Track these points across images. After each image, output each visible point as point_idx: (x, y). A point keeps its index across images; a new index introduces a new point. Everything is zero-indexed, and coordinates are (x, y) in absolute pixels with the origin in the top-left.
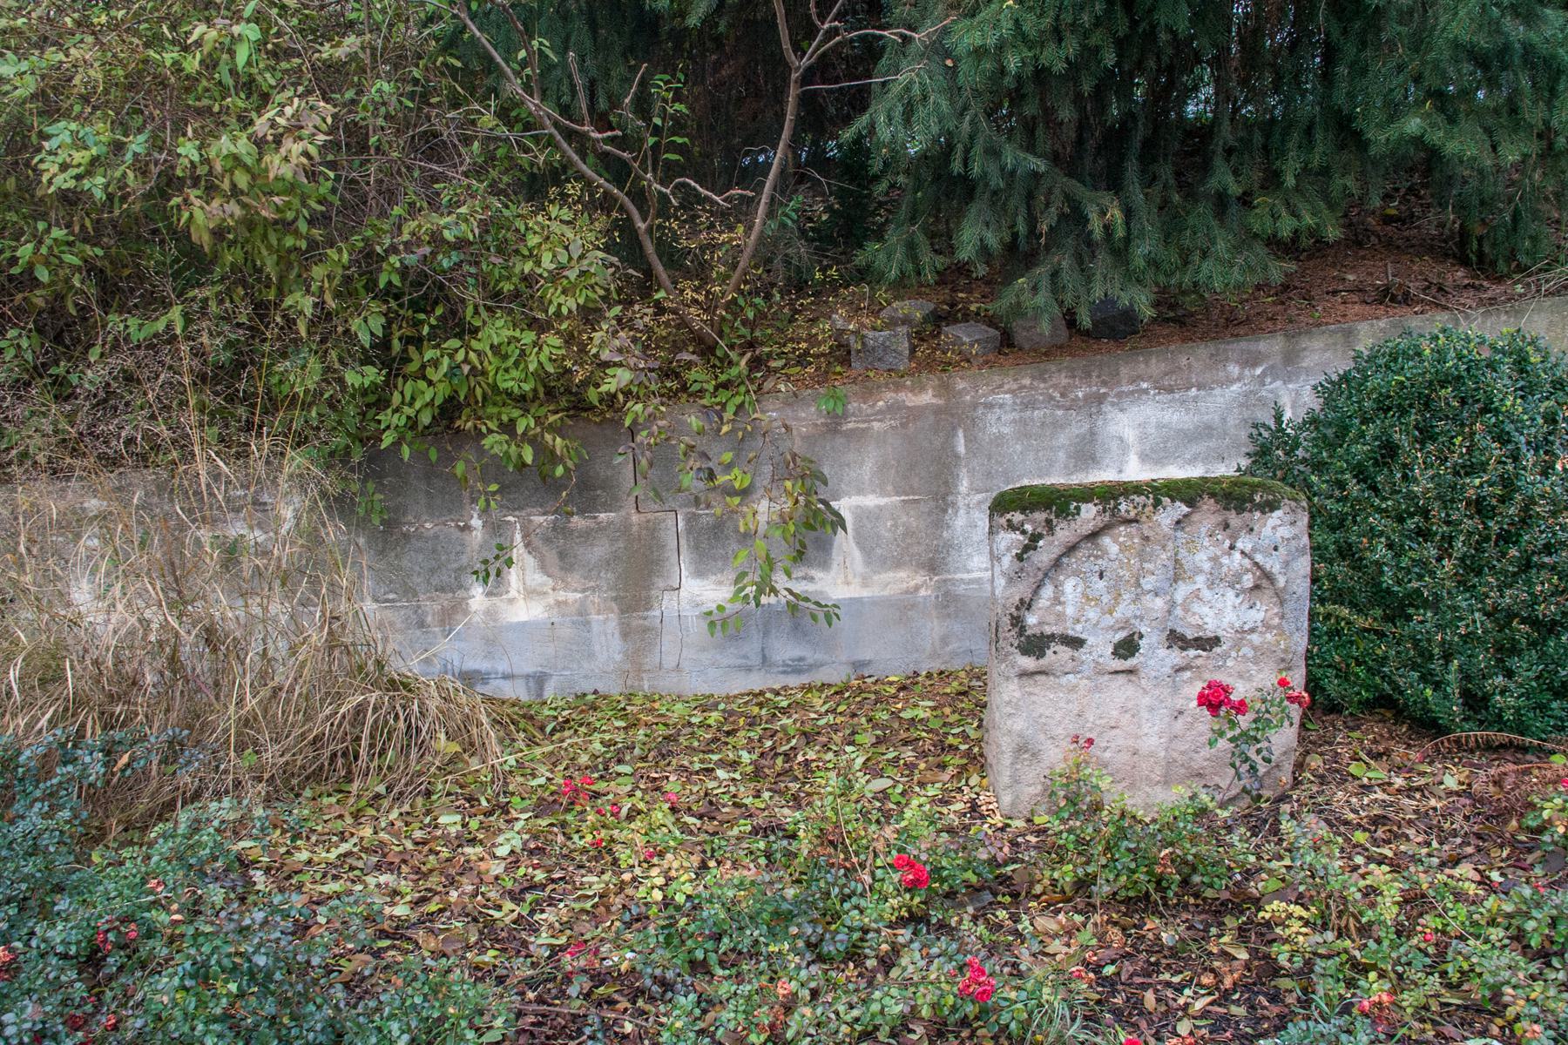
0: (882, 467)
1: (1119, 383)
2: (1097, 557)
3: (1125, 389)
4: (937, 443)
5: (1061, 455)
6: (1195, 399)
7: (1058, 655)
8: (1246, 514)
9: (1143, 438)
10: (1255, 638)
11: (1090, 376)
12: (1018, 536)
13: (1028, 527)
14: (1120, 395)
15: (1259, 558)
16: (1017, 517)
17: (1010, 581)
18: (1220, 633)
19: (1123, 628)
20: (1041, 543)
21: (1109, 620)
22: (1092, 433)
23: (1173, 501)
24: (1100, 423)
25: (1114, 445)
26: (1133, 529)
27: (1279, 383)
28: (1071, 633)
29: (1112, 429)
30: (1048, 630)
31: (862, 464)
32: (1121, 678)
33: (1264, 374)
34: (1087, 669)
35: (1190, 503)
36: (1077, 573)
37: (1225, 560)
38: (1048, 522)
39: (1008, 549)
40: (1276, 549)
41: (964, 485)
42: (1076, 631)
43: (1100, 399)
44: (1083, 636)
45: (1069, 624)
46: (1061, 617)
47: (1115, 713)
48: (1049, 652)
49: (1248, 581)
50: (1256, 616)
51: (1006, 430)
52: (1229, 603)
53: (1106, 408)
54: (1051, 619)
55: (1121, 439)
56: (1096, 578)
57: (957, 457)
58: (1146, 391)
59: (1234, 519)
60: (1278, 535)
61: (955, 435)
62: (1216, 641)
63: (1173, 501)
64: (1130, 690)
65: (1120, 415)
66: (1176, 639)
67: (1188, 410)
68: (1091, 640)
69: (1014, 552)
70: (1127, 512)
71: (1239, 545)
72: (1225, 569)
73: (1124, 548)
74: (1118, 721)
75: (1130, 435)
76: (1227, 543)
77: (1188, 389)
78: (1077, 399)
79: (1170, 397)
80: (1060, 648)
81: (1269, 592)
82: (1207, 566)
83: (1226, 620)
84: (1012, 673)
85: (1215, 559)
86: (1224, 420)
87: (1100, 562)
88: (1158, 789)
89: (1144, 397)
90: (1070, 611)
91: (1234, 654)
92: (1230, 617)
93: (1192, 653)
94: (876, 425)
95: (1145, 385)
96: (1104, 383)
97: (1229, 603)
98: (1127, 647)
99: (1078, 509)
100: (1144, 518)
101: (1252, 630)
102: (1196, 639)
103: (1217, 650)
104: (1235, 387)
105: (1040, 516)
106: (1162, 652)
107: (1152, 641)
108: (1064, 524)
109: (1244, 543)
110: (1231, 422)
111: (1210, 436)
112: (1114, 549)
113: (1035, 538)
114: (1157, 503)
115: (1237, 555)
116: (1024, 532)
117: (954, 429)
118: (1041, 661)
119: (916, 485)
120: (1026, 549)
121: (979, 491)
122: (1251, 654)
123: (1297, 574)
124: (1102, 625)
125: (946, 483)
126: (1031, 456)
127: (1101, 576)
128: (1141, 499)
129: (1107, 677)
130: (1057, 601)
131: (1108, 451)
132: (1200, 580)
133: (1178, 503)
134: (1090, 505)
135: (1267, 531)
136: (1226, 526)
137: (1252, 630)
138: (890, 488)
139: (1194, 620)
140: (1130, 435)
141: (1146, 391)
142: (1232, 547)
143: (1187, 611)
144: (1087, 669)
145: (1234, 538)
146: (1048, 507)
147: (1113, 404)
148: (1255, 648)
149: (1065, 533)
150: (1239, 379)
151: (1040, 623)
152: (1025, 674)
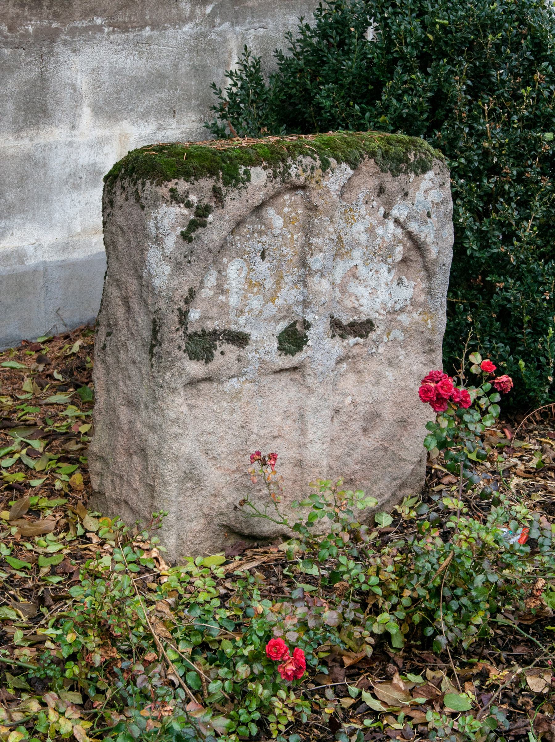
1: (71, 17)
2: (261, 233)
3: (78, 24)
5: (10, 106)
6: (149, 41)
7: (226, 355)
8: (402, 176)
9: (97, 86)
10: (403, 318)
11: (40, 6)
12: (180, 210)
13: (193, 198)
14: (73, 32)
15: (413, 227)
16: (182, 186)
17: (178, 267)
18: (374, 316)
19: (284, 317)
20: (210, 218)
21: (271, 309)
22: (43, 79)
23: (339, 163)
24: (51, 66)
25: (66, 94)
26: (297, 197)
27: (227, 25)
28: (233, 327)
29: (64, 74)
30: (210, 326)
32: (285, 378)
33: (213, 13)
34: (252, 370)
36: (240, 254)
37: (380, 231)
38: (216, 191)
39: (173, 228)
40: (429, 216)
42: (239, 325)
43: (51, 36)
44: (246, 330)
45: (232, 317)
46: (224, 308)
47: (278, 420)
48: (217, 353)
49: (399, 252)
50: (405, 293)
52: (383, 281)
53: (59, 47)
54: (214, 311)
55: (74, 87)
56: (258, 259)
58: (99, 29)
59: (391, 183)
60: (429, 199)
62: (154, 322)
64: (292, 392)
65: (73, 58)
66: (339, 329)
67: (141, 53)
68: (255, 335)
69: (179, 230)
70: (298, 176)
71: (395, 212)
72: (379, 241)
73: (288, 221)
74: (281, 428)
75: (83, 82)
76: (382, 210)
77: (142, 27)
78: (26, 35)
79: (124, 36)
80: (228, 347)
81: (418, 266)
82: (363, 239)
83: (379, 300)
84: (179, 383)
85: (370, 230)
86: (175, 66)
87: (264, 238)
88: (140, 493)
89: (98, 36)
90: (234, 300)
91: (385, 339)
92: (383, 296)
93: (352, 340)
95: (98, 21)
96: (56, 16)
97: (383, 281)
98: (293, 339)
99: (247, 173)
100: (313, 184)
101: (402, 310)
102: (352, 325)
104: (187, 28)
105: (206, 184)
106: (328, 343)
107: (318, 331)
108: (234, 194)
109: (400, 211)
110: (183, 69)
111: (162, 86)
112: (278, 222)
113: (202, 212)
114: (325, 165)
115: (391, 224)
116: (188, 205)
118: (211, 366)
120: (193, 225)
122: (401, 337)
123: (440, 243)
124: (264, 316)
127: (263, 257)
128: (307, 161)
129: (271, 377)
130: (221, 289)
131: (59, 102)
132: (357, 254)
133: (344, 165)
134: (259, 169)
135: (420, 195)
136: (381, 191)
137: (402, 310)
139: (349, 302)
140: (83, 82)
141: (99, 29)
142: (386, 215)
143: (344, 292)
144: (252, 370)
145: (389, 205)
146: (212, 172)
147: (66, 43)
148: (404, 330)
149: (235, 204)
150: (191, 18)
151: (203, 318)
152: (193, 383)
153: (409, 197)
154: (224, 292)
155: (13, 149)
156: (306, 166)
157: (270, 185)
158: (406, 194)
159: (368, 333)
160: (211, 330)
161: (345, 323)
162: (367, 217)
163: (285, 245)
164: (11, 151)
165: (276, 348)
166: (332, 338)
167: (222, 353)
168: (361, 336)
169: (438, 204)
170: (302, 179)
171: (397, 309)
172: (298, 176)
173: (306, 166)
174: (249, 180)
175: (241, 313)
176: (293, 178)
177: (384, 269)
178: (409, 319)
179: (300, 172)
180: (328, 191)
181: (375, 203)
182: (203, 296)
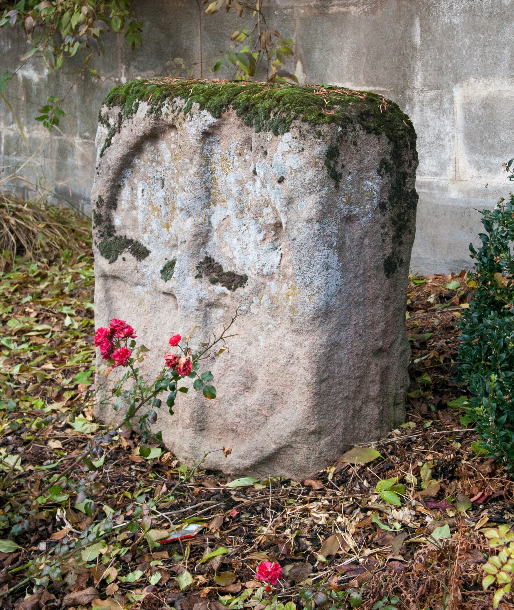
0: (357, 55)
4: (399, 32)
18: (248, 273)
31: (342, 49)
35: (218, 112)
40: (281, 180)
41: (418, 81)
42: (144, 240)
44: (149, 248)
48: (120, 257)
51: (457, 21)
54: (129, 223)
57: (414, 48)
61: (412, 24)
62: (242, 280)
63: (202, 108)
93: (219, 288)
94: (352, 9)
103: (240, 291)
117: (412, 17)
119: (381, 76)
121: (431, 88)
125: (404, 75)
126: (478, 53)
138: (361, 77)
153: (268, 157)
154: (135, 208)
155: (507, 93)
156: (177, 107)
157: (147, 119)
158: (266, 153)
159: (236, 287)
160: (130, 238)
161: (225, 271)
162: (239, 169)
163: (173, 179)
164: (506, 95)
165: (159, 270)
166: (196, 277)
167: (124, 259)
168: (229, 288)
169: (296, 171)
170: (170, 118)
171: (265, 272)
172: (167, 115)
173: (177, 107)
174: (136, 113)
175: (145, 230)
176: (163, 116)
177: (253, 228)
178: (277, 289)
179: (169, 112)
180: (187, 134)
181: (247, 157)
182: (123, 207)
